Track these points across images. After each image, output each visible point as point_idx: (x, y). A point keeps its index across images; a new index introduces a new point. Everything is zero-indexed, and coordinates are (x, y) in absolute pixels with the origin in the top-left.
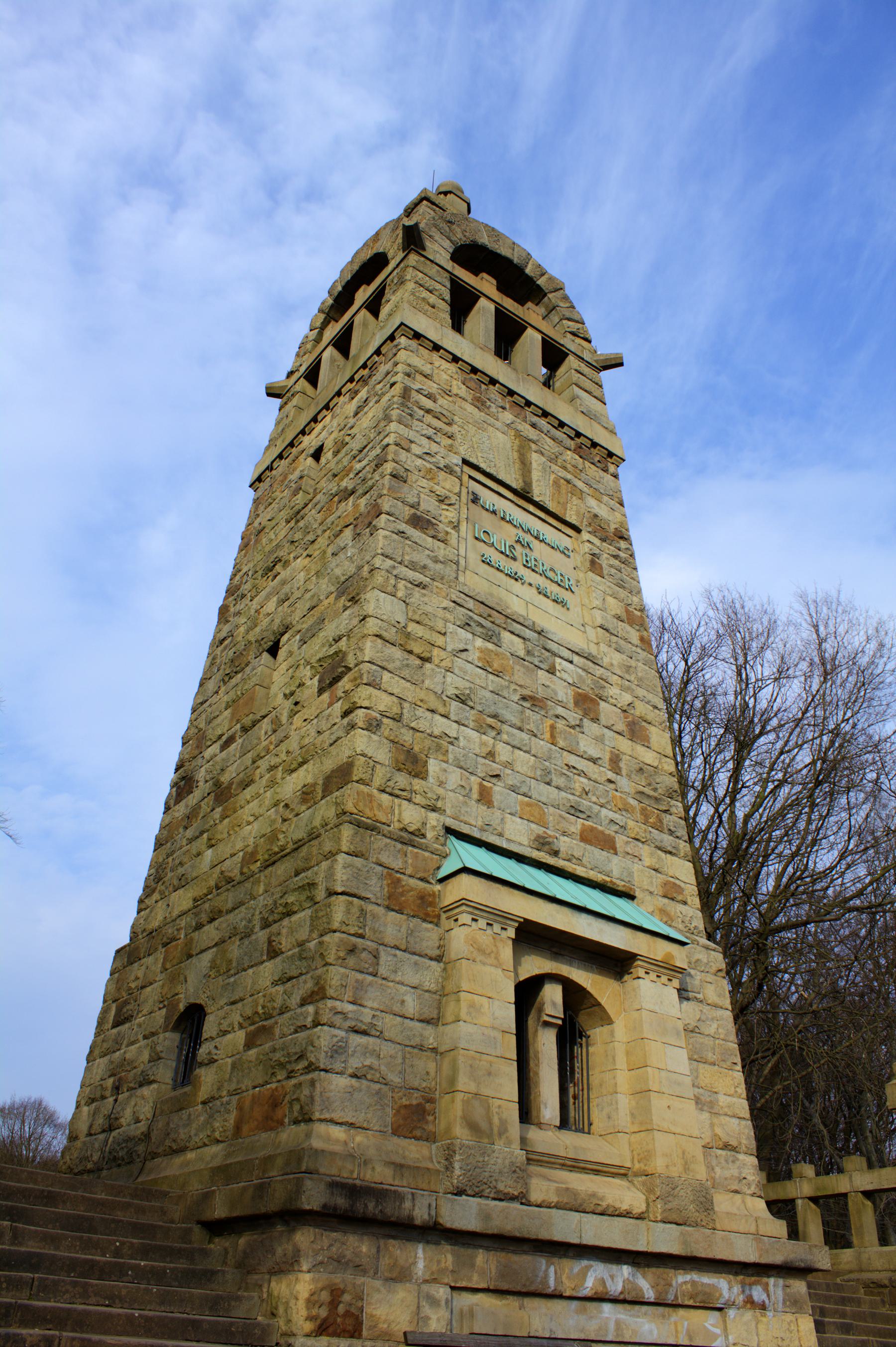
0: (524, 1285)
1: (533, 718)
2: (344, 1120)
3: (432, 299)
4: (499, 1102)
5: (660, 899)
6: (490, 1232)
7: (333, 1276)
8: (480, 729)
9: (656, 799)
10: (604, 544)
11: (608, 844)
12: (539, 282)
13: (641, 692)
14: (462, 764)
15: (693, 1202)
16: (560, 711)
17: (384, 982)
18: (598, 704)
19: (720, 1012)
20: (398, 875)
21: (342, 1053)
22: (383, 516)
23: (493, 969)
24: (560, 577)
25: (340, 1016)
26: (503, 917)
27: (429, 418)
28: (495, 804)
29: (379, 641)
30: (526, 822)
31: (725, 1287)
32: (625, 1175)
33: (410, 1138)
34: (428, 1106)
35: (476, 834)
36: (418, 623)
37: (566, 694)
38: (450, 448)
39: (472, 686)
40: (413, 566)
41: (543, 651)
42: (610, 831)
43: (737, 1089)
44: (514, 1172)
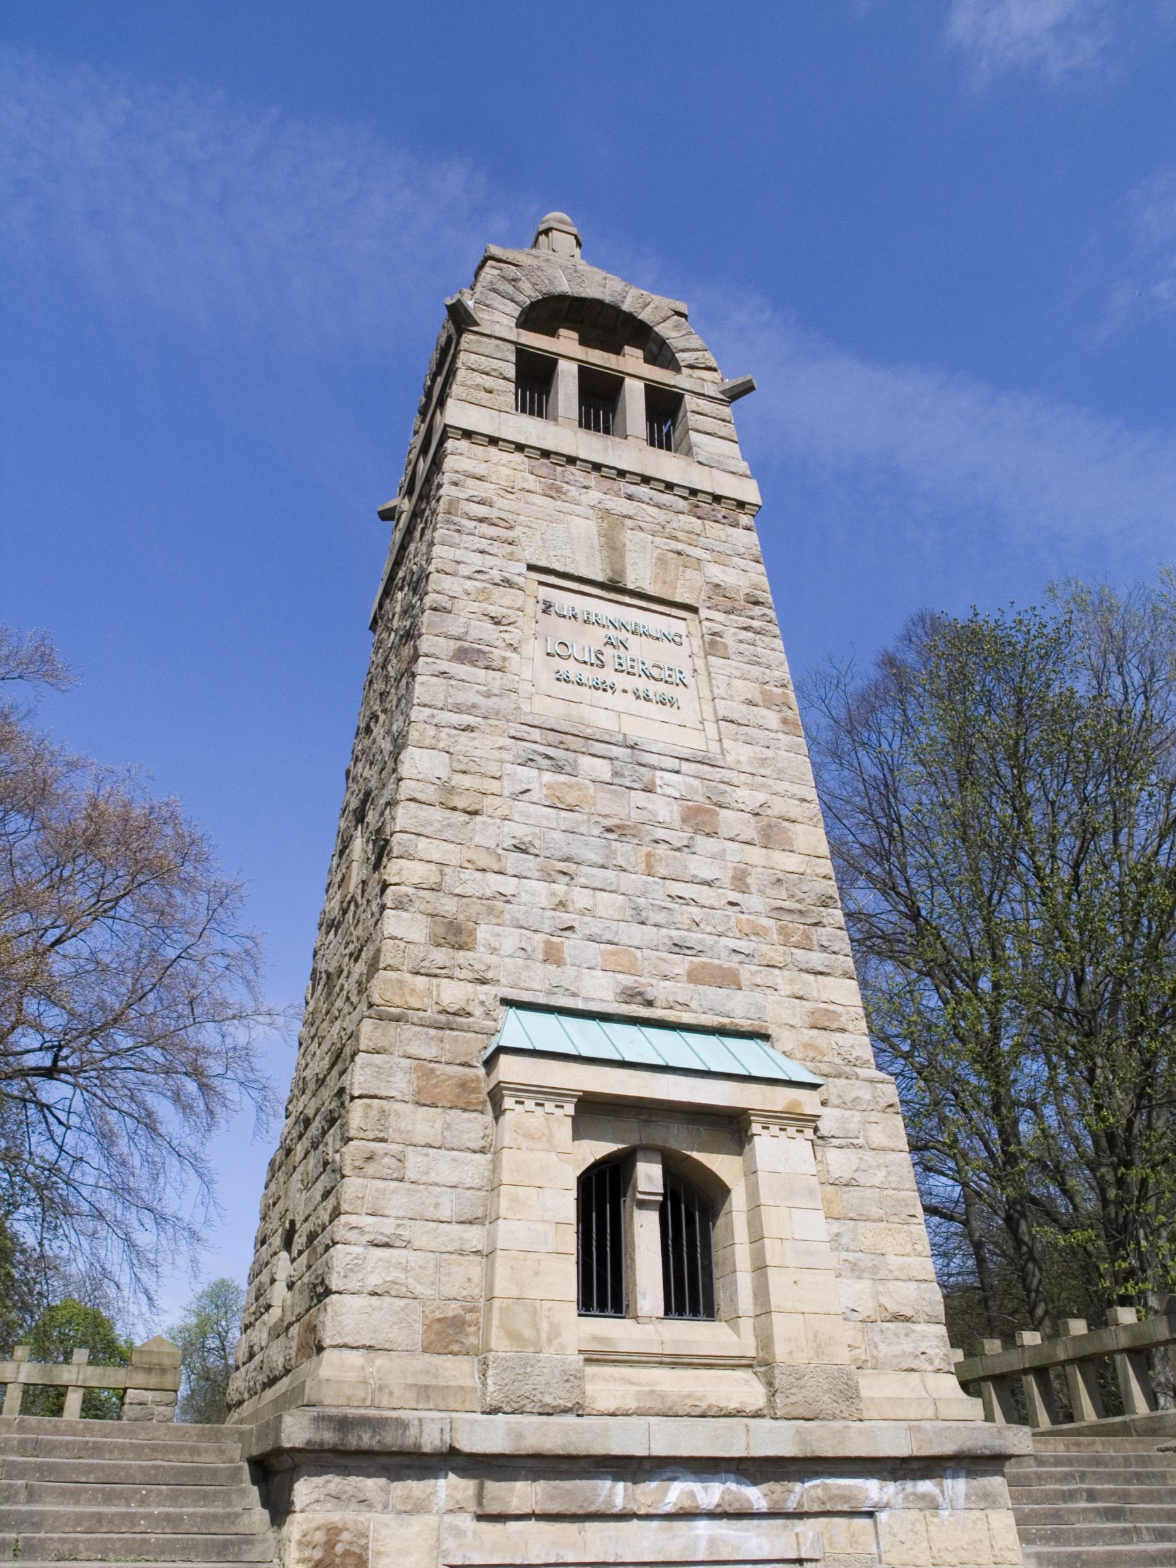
0: (581, 1507)
1: (623, 851)
3: (489, 382)
4: (549, 1304)
5: (806, 1031)
6: (522, 1452)
7: (330, 1514)
8: (547, 878)
9: (801, 912)
10: (732, 617)
11: (730, 980)
12: (640, 317)
13: (781, 787)
14: (523, 923)
15: (829, 1390)
16: (661, 833)
17: (413, 1186)
18: (718, 814)
19: (891, 1156)
20: (432, 1065)
22: (421, 659)
23: (543, 1154)
24: (668, 672)
25: (355, 1231)
27: (485, 529)
28: (568, 961)
29: (412, 804)
30: (611, 974)
31: (872, 1489)
32: (750, 1366)
35: (542, 999)
36: (465, 772)
37: (671, 812)
38: (511, 557)
39: (537, 830)
40: (458, 709)
41: (637, 767)
42: (733, 962)
43: (916, 1247)
44: (567, 1381)
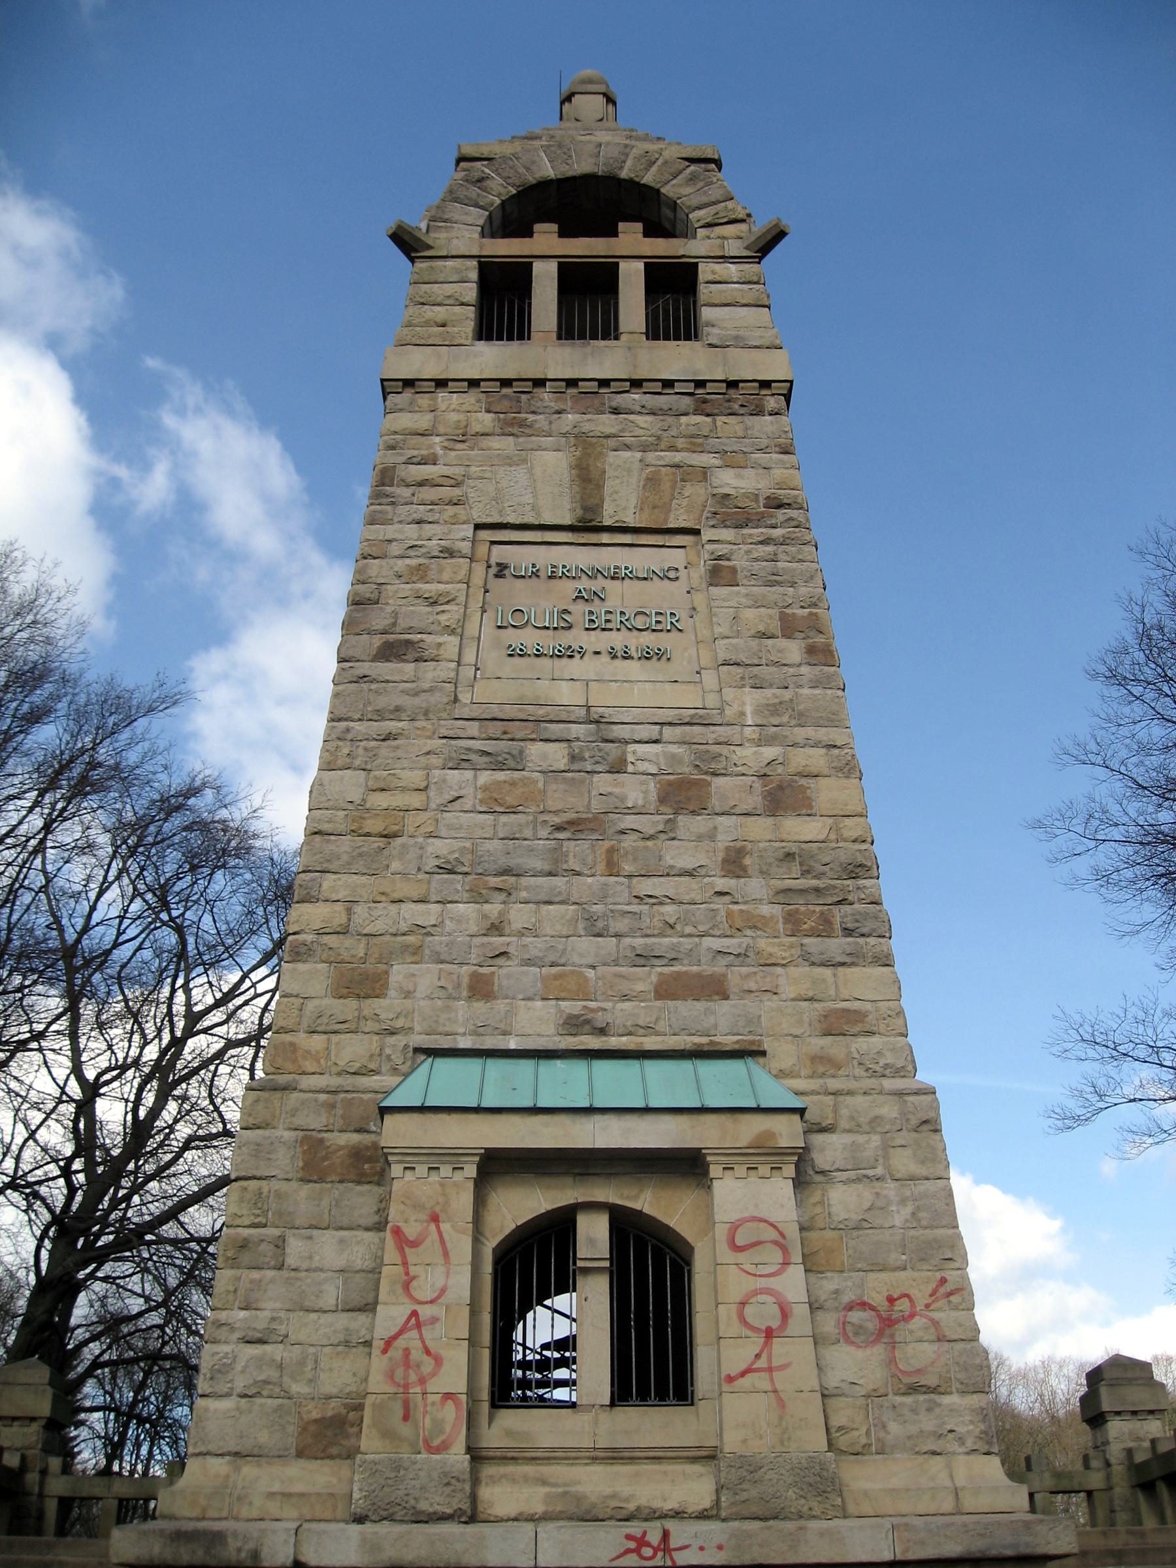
1: (577, 850)
2: (225, 1450)
8: (477, 897)
11: (715, 989)
15: (795, 1484)
21: (228, 1372)
25: (225, 1328)
26: (453, 1156)
30: (553, 1002)
33: (322, 1458)
34: (352, 1415)
42: (719, 967)
44: (448, 1484)
